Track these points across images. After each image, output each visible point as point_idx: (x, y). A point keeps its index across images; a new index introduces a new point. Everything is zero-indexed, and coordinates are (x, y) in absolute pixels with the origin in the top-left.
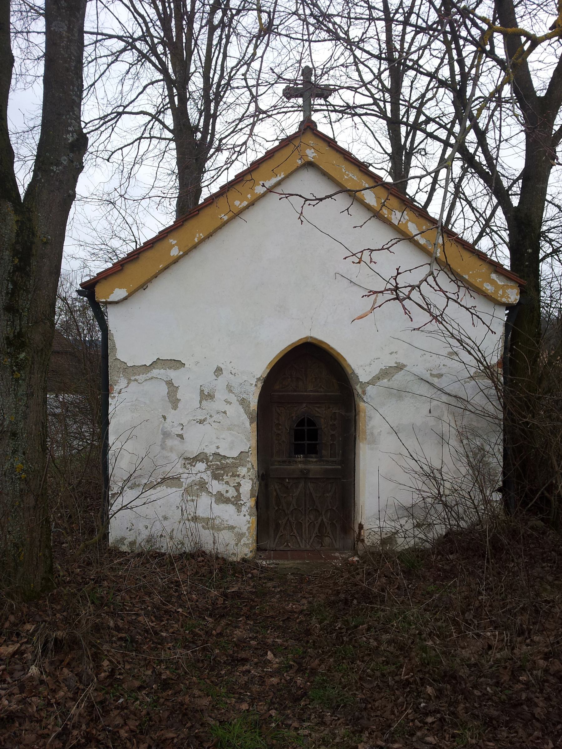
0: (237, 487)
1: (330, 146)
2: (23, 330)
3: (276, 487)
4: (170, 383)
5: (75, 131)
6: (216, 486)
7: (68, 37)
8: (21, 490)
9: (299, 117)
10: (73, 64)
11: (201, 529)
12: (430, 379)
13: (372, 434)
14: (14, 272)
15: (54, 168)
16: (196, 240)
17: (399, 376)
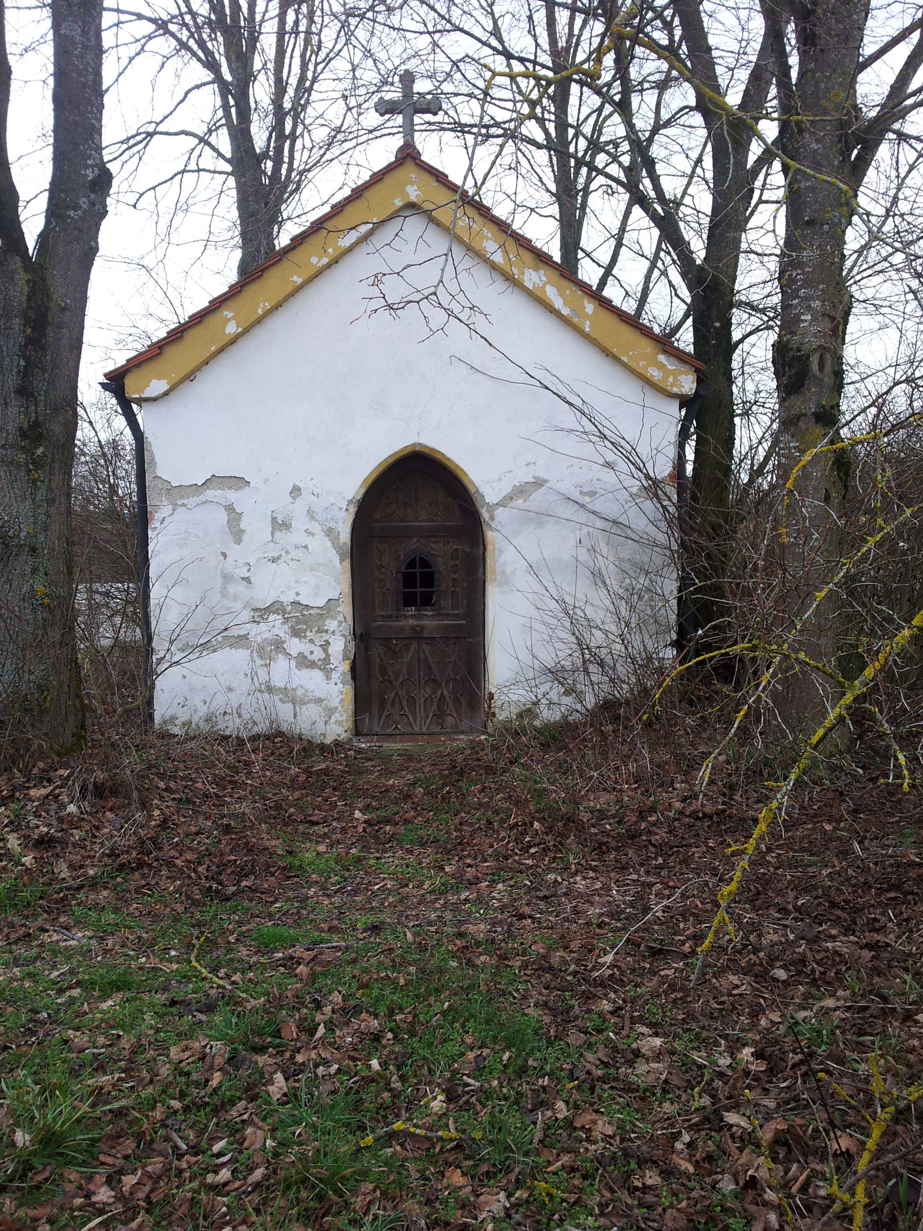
0: (325, 646)
1: (438, 181)
2: (40, 418)
3: (381, 651)
4: (230, 509)
5: (96, 165)
6: (295, 646)
7: (83, 43)
8: (44, 620)
9: (398, 142)
10: (91, 78)
11: (278, 703)
12: (580, 499)
13: (504, 573)
14: (26, 345)
15: (72, 213)
16: (260, 312)
17: (539, 495)
